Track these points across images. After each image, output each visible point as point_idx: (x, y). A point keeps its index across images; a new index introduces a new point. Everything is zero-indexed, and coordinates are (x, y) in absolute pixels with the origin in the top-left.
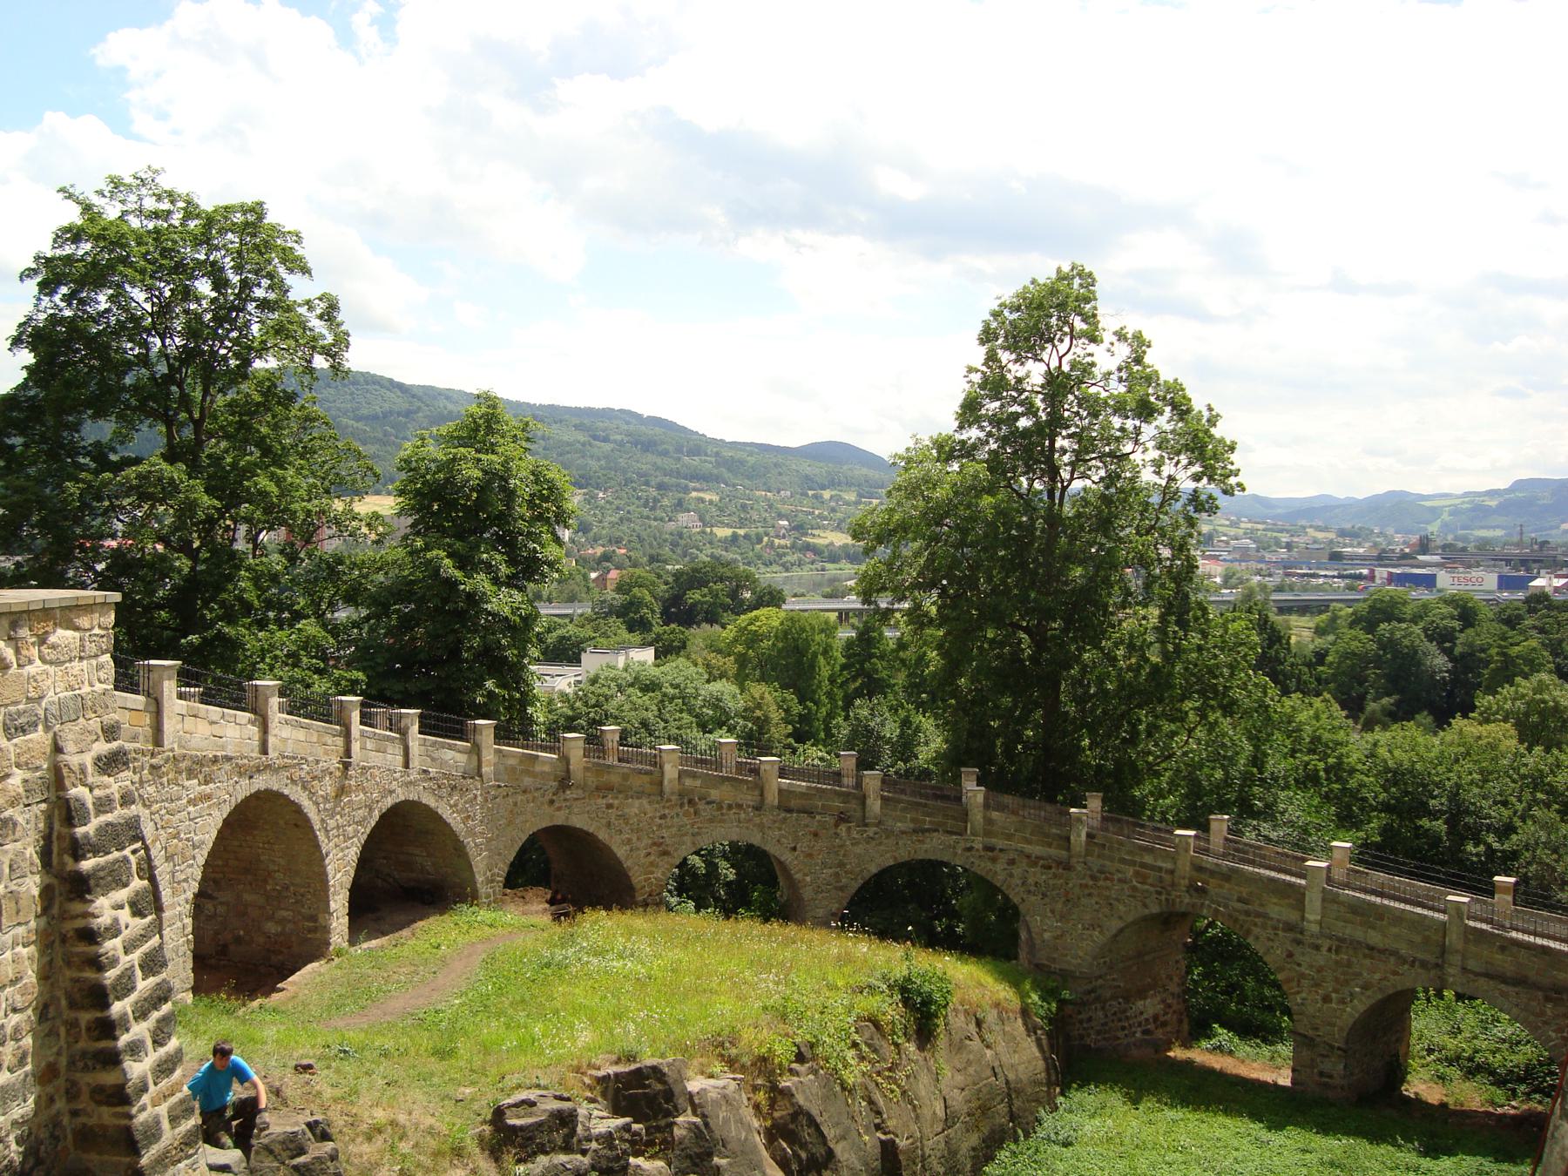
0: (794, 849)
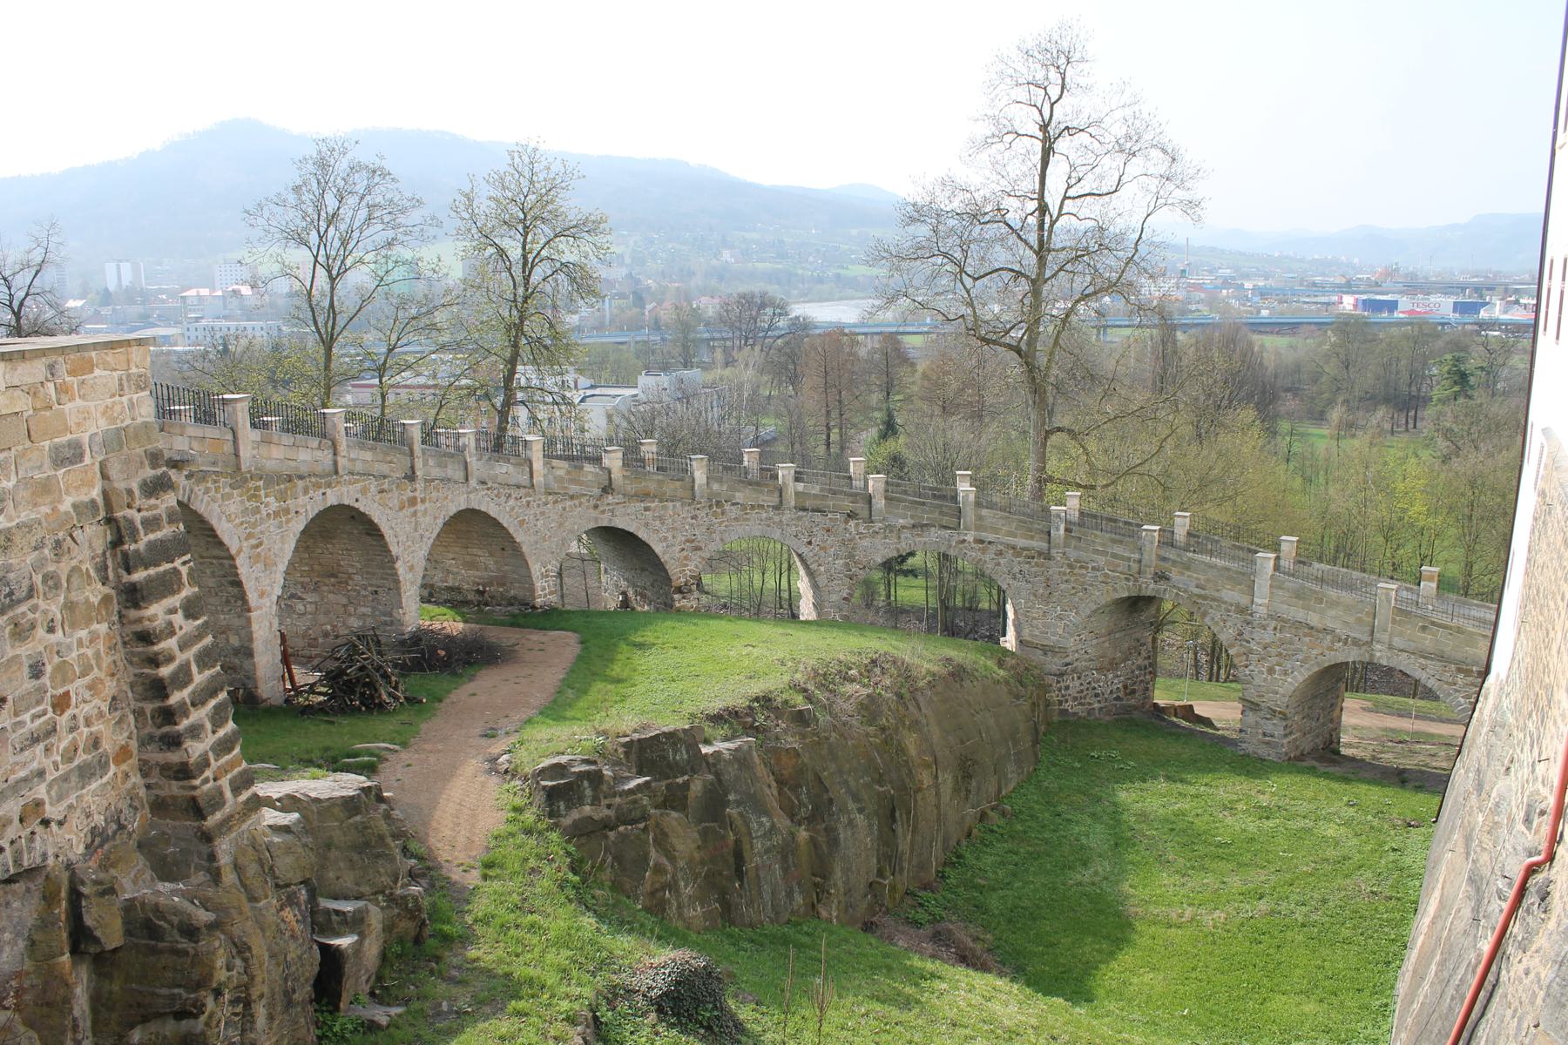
0: (810, 543)
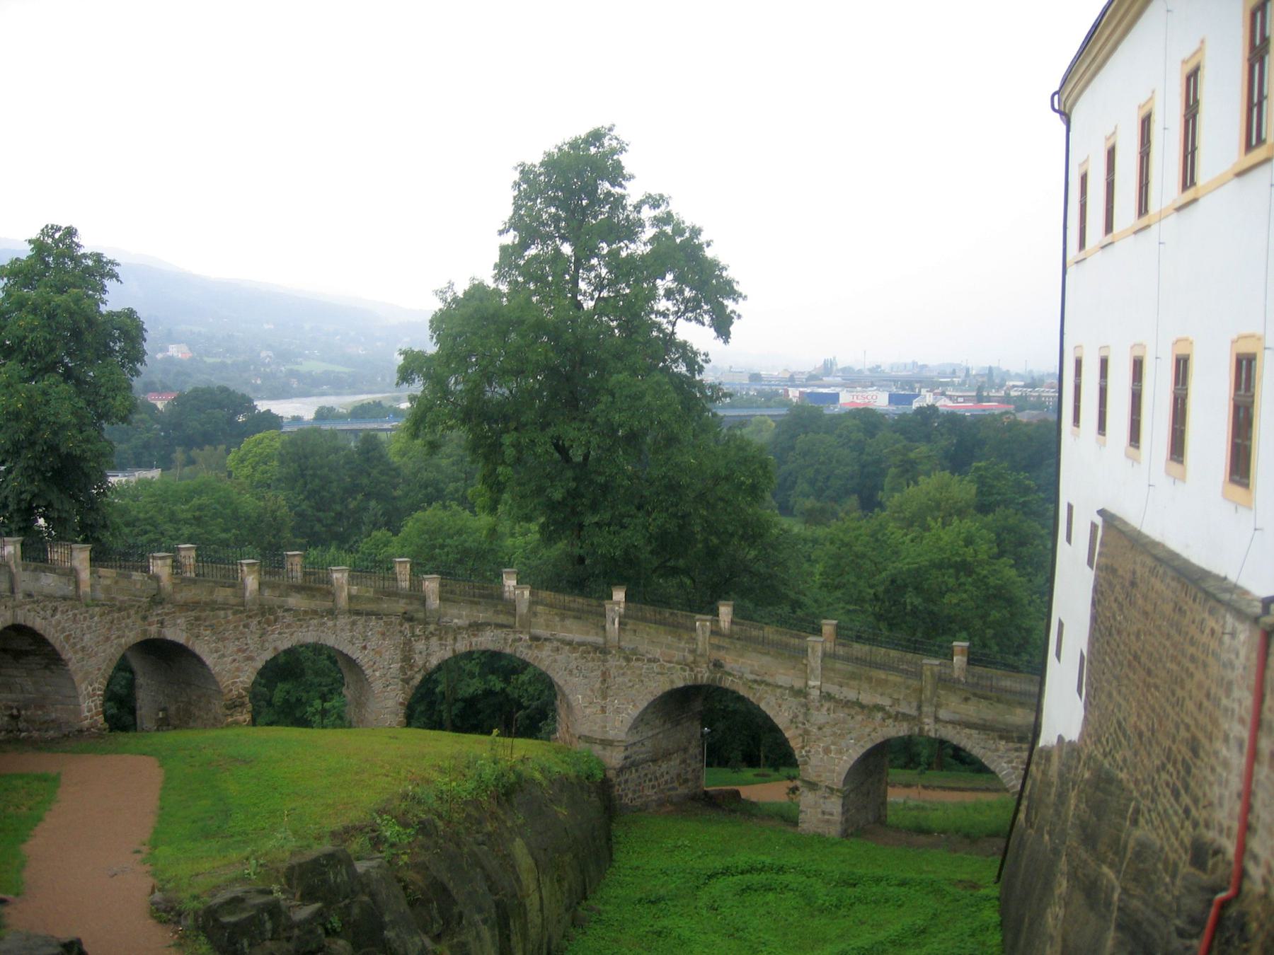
0: (365, 648)
